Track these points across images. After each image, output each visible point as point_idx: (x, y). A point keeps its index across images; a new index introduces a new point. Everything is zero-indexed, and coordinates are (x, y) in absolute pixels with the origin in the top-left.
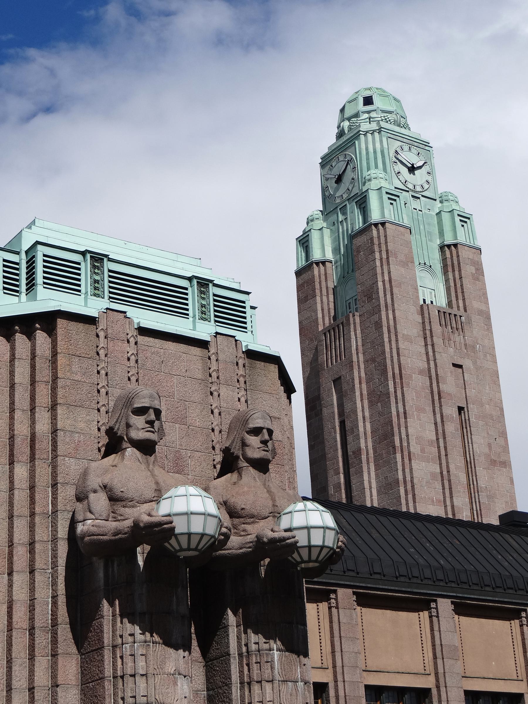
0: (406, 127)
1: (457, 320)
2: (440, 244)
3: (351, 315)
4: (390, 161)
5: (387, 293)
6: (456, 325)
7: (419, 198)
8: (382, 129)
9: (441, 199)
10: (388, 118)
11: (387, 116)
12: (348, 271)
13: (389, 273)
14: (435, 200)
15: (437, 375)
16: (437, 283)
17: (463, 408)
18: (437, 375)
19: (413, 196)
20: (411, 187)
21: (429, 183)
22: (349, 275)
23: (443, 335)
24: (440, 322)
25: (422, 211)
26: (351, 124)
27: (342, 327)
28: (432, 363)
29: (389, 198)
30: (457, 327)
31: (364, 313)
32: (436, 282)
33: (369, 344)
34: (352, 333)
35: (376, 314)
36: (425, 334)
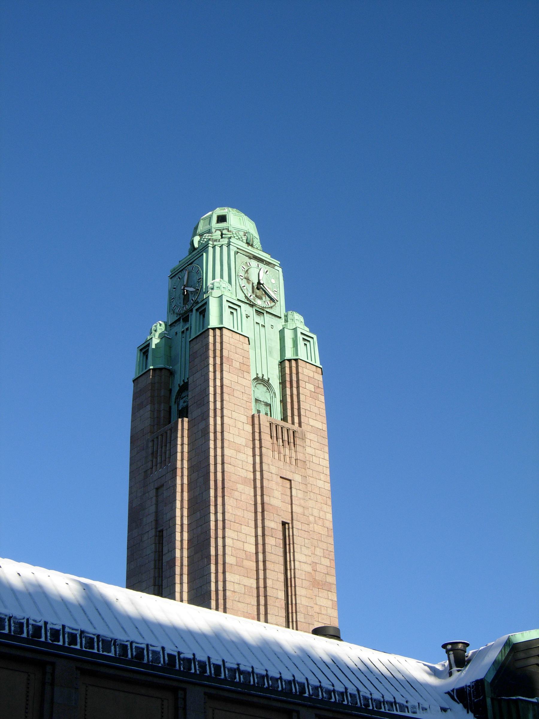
3: (180, 420)
14: (280, 318)
17: (288, 524)
28: (258, 474)
29: (230, 307)
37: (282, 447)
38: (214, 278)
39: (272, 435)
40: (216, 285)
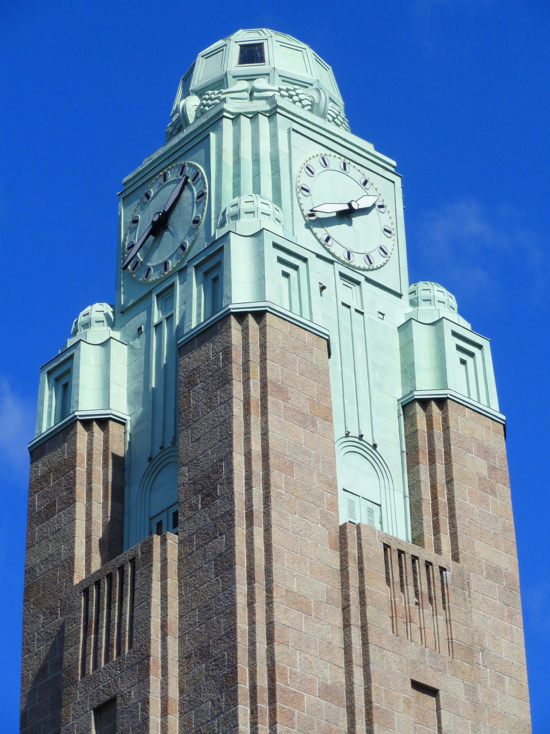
0: (340, 123)
1: (431, 577)
2: (402, 398)
3: (157, 539)
4: (291, 184)
5: (254, 483)
6: (429, 589)
7: (358, 283)
8: (279, 110)
9: (413, 296)
10: (297, 95)
11: (295, 90)
12: (163, 442)
13: (265, 434)
15: (368, 702)
16: (387, 490)
18: (368, 702)
19: (342, 275)
20: (341, 254)
21: (386, 254)
22: (165, 452)
23: (393, 607)
24: (387, 573)
25: (362, 313)
26: (204, 102)
27: (130, 569)
30: (430, 593)
31: (189, 536)
32: (387, 487)
33: (197, 613)
34: (156, 585)
35: (221, 534)
36: (346, 598)
37: (415, 610)
38: (237, 192)
39: (391, 578)
40: (244, 207)
